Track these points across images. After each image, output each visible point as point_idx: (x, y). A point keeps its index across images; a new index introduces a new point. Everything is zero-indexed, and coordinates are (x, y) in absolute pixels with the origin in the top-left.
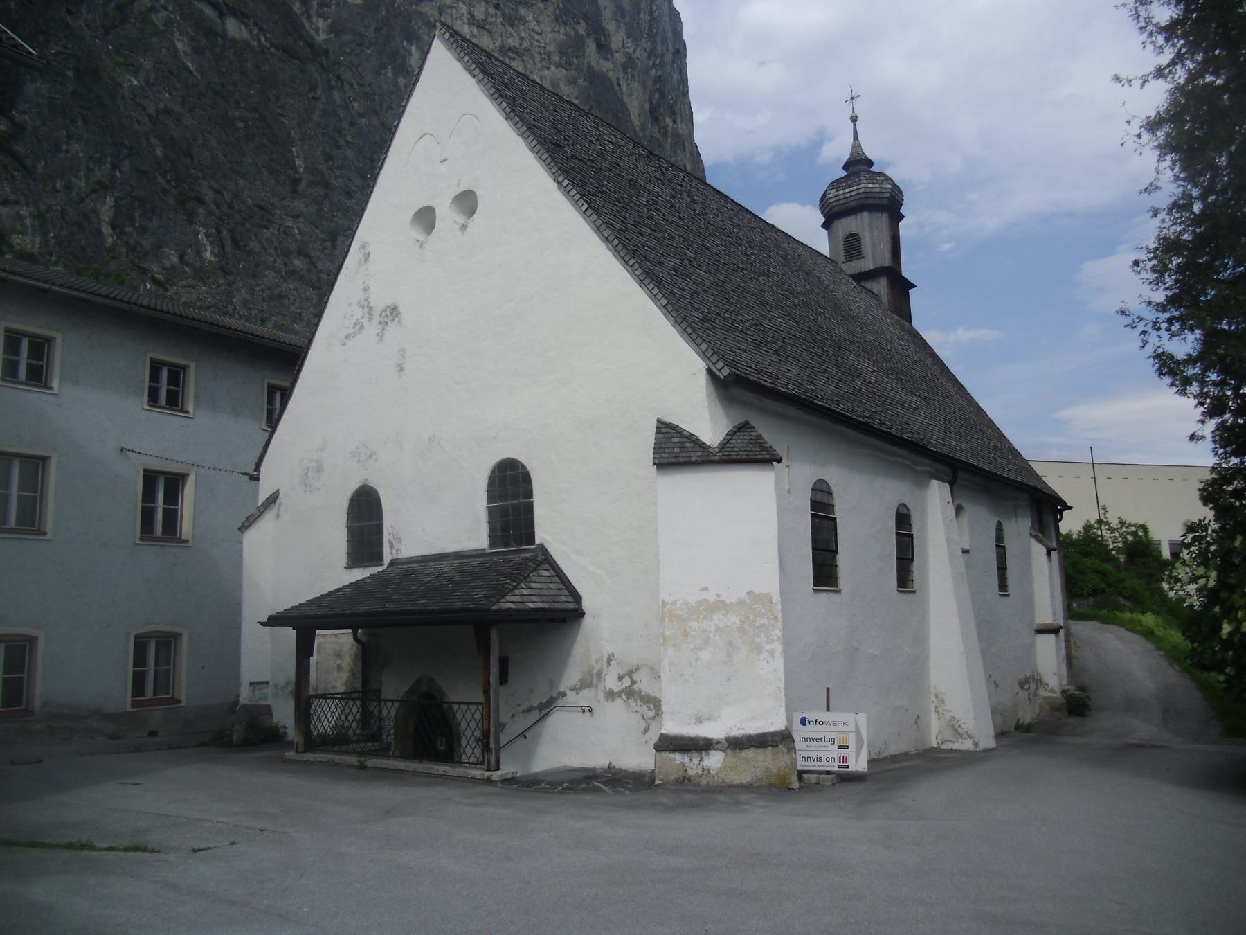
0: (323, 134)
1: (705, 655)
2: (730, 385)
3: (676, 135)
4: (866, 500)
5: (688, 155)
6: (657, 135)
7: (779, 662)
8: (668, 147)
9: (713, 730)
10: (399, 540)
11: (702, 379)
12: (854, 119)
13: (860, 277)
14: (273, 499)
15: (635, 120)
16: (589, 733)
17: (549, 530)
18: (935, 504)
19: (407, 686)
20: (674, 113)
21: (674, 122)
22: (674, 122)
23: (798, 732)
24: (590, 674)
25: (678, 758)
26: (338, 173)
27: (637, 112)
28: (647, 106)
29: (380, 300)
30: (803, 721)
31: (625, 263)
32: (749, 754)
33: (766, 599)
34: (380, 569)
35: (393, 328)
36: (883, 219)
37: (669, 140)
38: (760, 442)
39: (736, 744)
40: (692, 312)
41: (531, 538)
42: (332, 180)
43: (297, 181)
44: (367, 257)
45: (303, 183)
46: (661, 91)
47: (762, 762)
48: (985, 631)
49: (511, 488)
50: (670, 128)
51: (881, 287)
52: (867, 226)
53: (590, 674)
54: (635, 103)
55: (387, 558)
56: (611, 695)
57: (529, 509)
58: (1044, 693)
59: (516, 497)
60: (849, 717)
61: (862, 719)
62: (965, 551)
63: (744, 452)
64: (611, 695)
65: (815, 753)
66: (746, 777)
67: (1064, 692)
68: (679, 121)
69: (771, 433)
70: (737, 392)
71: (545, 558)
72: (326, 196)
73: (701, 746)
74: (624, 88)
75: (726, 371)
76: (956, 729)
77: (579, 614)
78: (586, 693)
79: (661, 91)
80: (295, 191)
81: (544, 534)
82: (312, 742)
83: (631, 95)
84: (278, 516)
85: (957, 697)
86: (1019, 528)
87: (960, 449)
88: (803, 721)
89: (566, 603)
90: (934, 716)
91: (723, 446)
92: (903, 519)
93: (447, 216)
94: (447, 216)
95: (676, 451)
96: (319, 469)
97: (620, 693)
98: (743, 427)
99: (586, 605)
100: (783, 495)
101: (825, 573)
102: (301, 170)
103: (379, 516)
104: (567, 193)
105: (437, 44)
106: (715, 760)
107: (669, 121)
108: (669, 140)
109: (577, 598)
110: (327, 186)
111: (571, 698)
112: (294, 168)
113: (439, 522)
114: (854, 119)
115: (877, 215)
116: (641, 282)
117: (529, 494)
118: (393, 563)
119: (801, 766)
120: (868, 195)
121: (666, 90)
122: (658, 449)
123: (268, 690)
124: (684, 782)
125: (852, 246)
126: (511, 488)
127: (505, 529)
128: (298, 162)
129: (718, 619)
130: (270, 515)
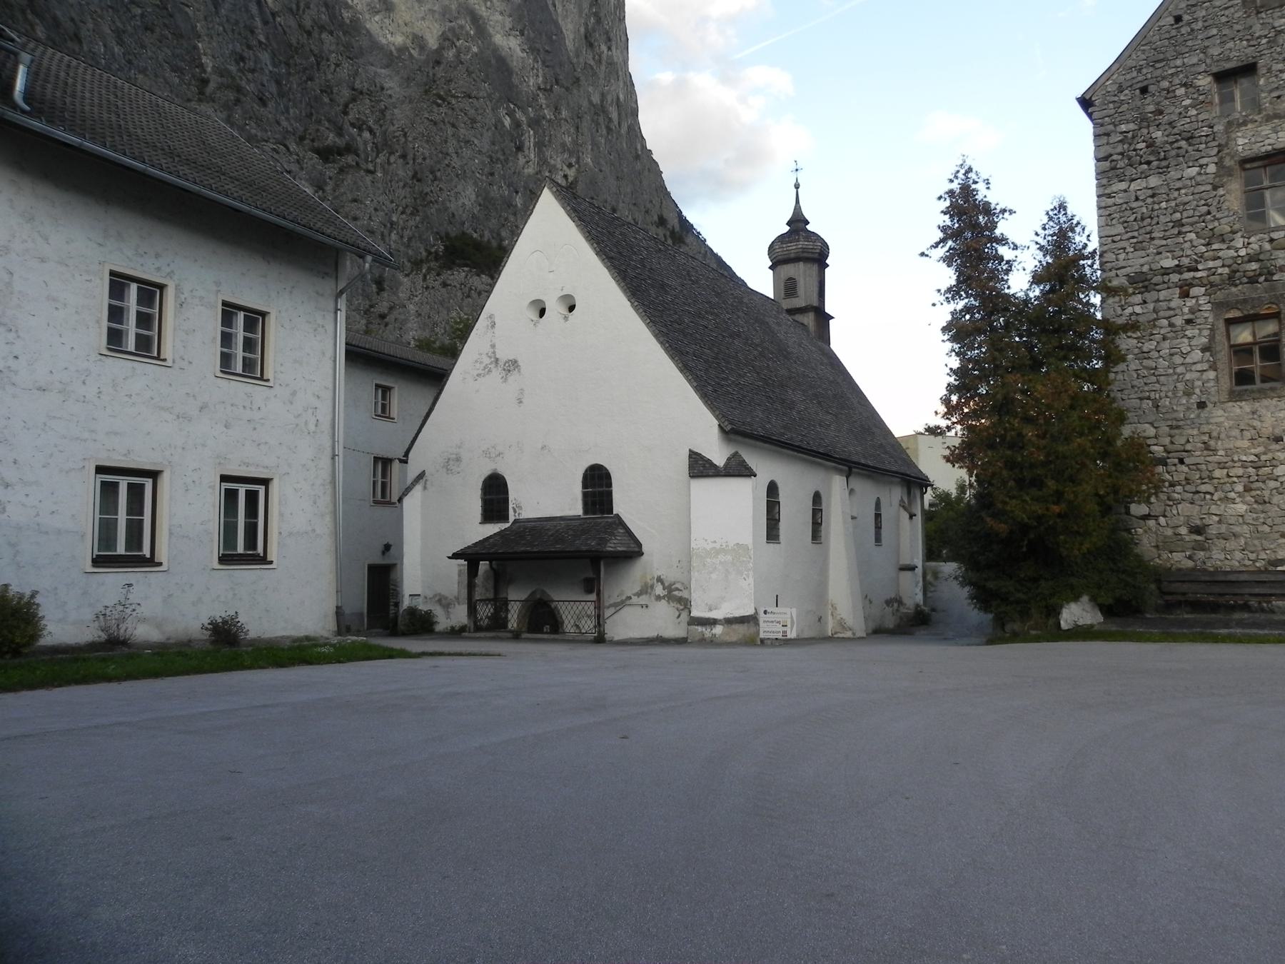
0: (233, 31)
1: (714, 576)
2: (730, 432)
3: (611, 63)
4: (797, 483)
5: (621, 84)
6: (592, 63)
7: (751, 580)
8: (602, 76)
9: (718, 614)
10: (520, 508)
11: (716, 430)
12: (797, 186)
13: (791, 312)
14: (421, 476)
15: (570, 44)
16: (639, 619)
17: (621, 506)
18: (836, 487)
19: (529, 592)
20: (609, 40)
21: (609, 49)
22: (609, 49)
23: (762, 617)
24: (646, 584)
25: (700, 629)
26: (250, 76)
27: (571, 37)
28: (582, 30)
29: (504, 355)
30: (765, 612)
31: (672, 358)
32: (735, 627)
33: (745, 548)
34: (507, 525)
35: (513, 377)
36: (815, 267)
37: (603, 68)
38: (743, 464)
39: (729, 621)
40: (710, 388)
41: (611, 511)
42: (243, 83)
43: (205, 82)
44: (493, 325)
45: (212, 86)
46: (596, 15)
47: (741, 630)
48: (862, 567)
49: (597, 482)
50: (604, 56)
51: (809, 319)
52: (799, 271)
53: (646, 584)
54: (570, 26)
55: (512, 519)
56: (659, 598)
57: (610, 494)
58: (903, 610)
59: (601, 486)
60: (788, 610)
61: (794, 611)
62: (853, 518)
63: (737, 469)
64: (659, 598)
65: (767, 629)
66: (734, 639)
67: (917, 606)
68: (614, 48)
69: (752, 459)
70: (732, 436)
71: (620, 522)
72: (238, 101)
73: (712, 622)
74: (559, 10)
75: (729, 427)
76: (842, 624)
77: (640, 554)
78: (644, 597)
79: (596, 15)
80: (201, 93)
81: (619, 507)
82: (478, 629)
83: (566, 16)
84: (425, 488)
85: (844, 604)
86: (893, 496)
87: (855, 451)
88: (765, 612)
89: (634, 548)
90: (830, 618)
91: (726, 465)
92: (817, 498)
93: (555, 309)
94: (555, 309)
95: (700, 467)
96: (458, 459)
97: (664, 597)
98: (736, 455)
99: (644, 549)
100: (755, 489)
101: (772, 533)
102: (209, 69)
103: (506, 492)
104: (636, 310)
105: (546, 191)
106: (718, 630)
107: (604, 48)
108: (603, 68)
109: (640, 545)
110: (239, 89)
111: (635, 600)
112: (201, 66)
113: (547, 496)
114: (797, 186)
115: (809, 265)
116: (681, 371)
117: (610, 485)
118: (516, 521)
119: (762, 635)
120: (804, 250)
121: (602, 15)
122: (691, 467)
123: (420, 600)
124: (703, 642)
125: (788, 287)
126: (597, 482)
127: (594, 504)
128: (204, 60)
129: (721, 557)
130: (419, 487)
